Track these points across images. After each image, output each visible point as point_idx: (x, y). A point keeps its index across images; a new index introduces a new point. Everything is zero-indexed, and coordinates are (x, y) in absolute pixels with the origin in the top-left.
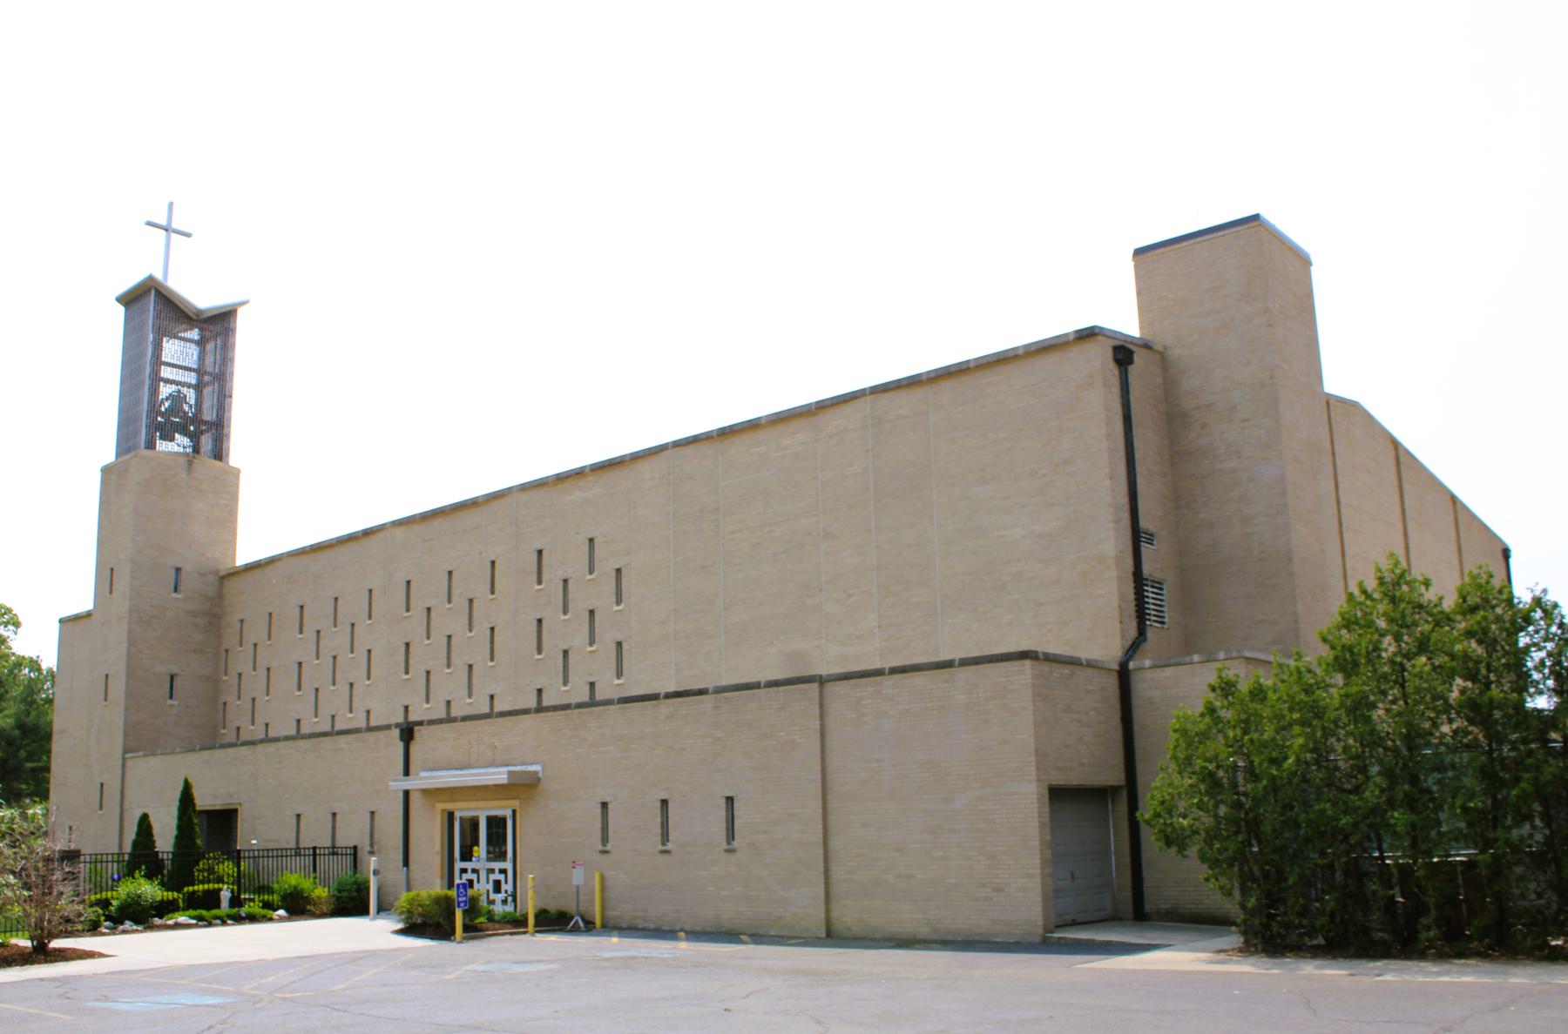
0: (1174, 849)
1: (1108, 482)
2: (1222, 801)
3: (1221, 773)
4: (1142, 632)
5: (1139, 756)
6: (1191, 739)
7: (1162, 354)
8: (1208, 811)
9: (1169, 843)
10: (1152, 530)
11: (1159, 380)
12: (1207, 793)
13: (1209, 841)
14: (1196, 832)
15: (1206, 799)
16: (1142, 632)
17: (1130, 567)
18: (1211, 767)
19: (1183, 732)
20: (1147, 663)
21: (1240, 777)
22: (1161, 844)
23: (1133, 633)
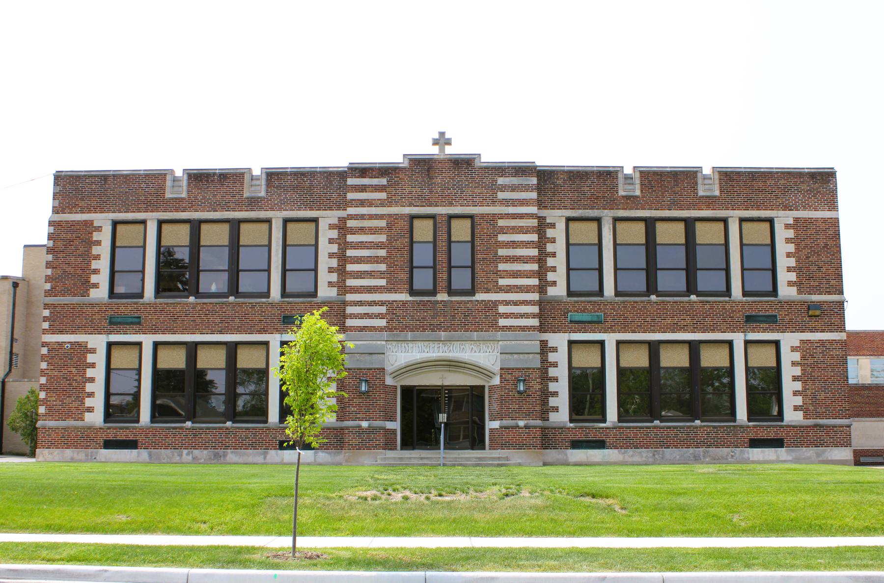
0: (14, 432)
1: (6, 324)
2: (28, 420)
3: (29, 413)
4: (10, 370)
5: (5, 407)
6: (22, 404)
7: (28, 281)
8: (24, 422)
9: (13, 430)
10: (17, 338)
11: (26, 290)
12: (25, 418)
13: (23, 430)
14: (20, 427)
15: (24, 419)
16: (10, 370)
17: (9, 350)
18: (26, 411)
19: (20, 402)
20: (11, 380)
21: (34, 414)
22: (11, 430)
23: (8, 370)
